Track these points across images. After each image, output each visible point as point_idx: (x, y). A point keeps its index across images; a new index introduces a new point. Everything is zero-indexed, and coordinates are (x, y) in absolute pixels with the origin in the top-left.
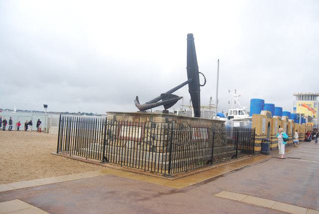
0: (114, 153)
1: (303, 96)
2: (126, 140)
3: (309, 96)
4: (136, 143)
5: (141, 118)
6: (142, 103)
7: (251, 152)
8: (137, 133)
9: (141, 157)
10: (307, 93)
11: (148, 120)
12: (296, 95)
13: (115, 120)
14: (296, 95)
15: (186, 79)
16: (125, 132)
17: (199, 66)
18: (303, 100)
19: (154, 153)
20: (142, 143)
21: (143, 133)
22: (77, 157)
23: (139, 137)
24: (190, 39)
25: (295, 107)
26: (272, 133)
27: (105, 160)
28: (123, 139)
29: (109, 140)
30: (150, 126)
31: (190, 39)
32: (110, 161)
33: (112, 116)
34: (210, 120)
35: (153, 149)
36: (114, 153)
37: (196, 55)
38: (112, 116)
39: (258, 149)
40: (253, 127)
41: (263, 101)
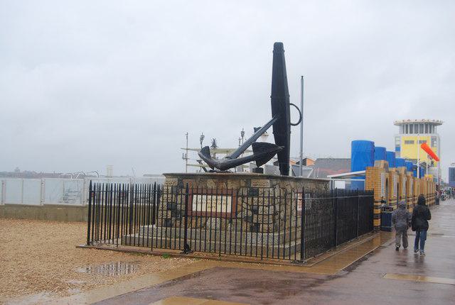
0: (196, 239)
1: (411, 125)
2: (206, 217)
3: (421, 125)
4: (224, 220)
5: (229, 183)
6: (221, 158)
7: (370, 228)
8: (224, 205)
9: (238, 241)
10: (413, 120)
11: (243, 184)
12: (400, 125)
13: (180, 186)
14: (400, 125)
15: (270, 118)
16: (200, 204)
17: (290, 94)
18: (411, 132)
19: (260, 234)
20: (234, 221)
21: (235, 205)
22: (159, 250)
23: (229, 211)
24: (278, 50)
25: (398, 143)
26: (390, 196)
27: (187, 249)
28: (200, 215)
29: (173, 219)
30: (245, 193)
31: (278, 50)
32: (193, 249)
33: (176, 179)
34: (308, 179)
35: (255, 228)
36: (196, 239)
37: (286, 77)
38: (176, 179)
39: (377, 223)
40: (367, 188)
41: (372, 143)
